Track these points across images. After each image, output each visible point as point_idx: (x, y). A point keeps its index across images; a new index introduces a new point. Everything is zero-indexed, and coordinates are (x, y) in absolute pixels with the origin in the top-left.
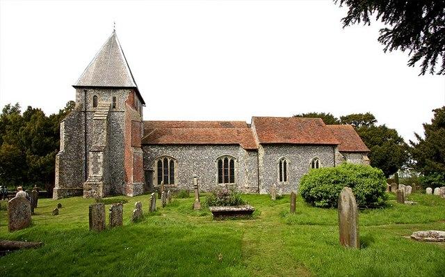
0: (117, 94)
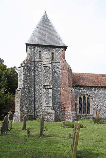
0: (55, 51)
